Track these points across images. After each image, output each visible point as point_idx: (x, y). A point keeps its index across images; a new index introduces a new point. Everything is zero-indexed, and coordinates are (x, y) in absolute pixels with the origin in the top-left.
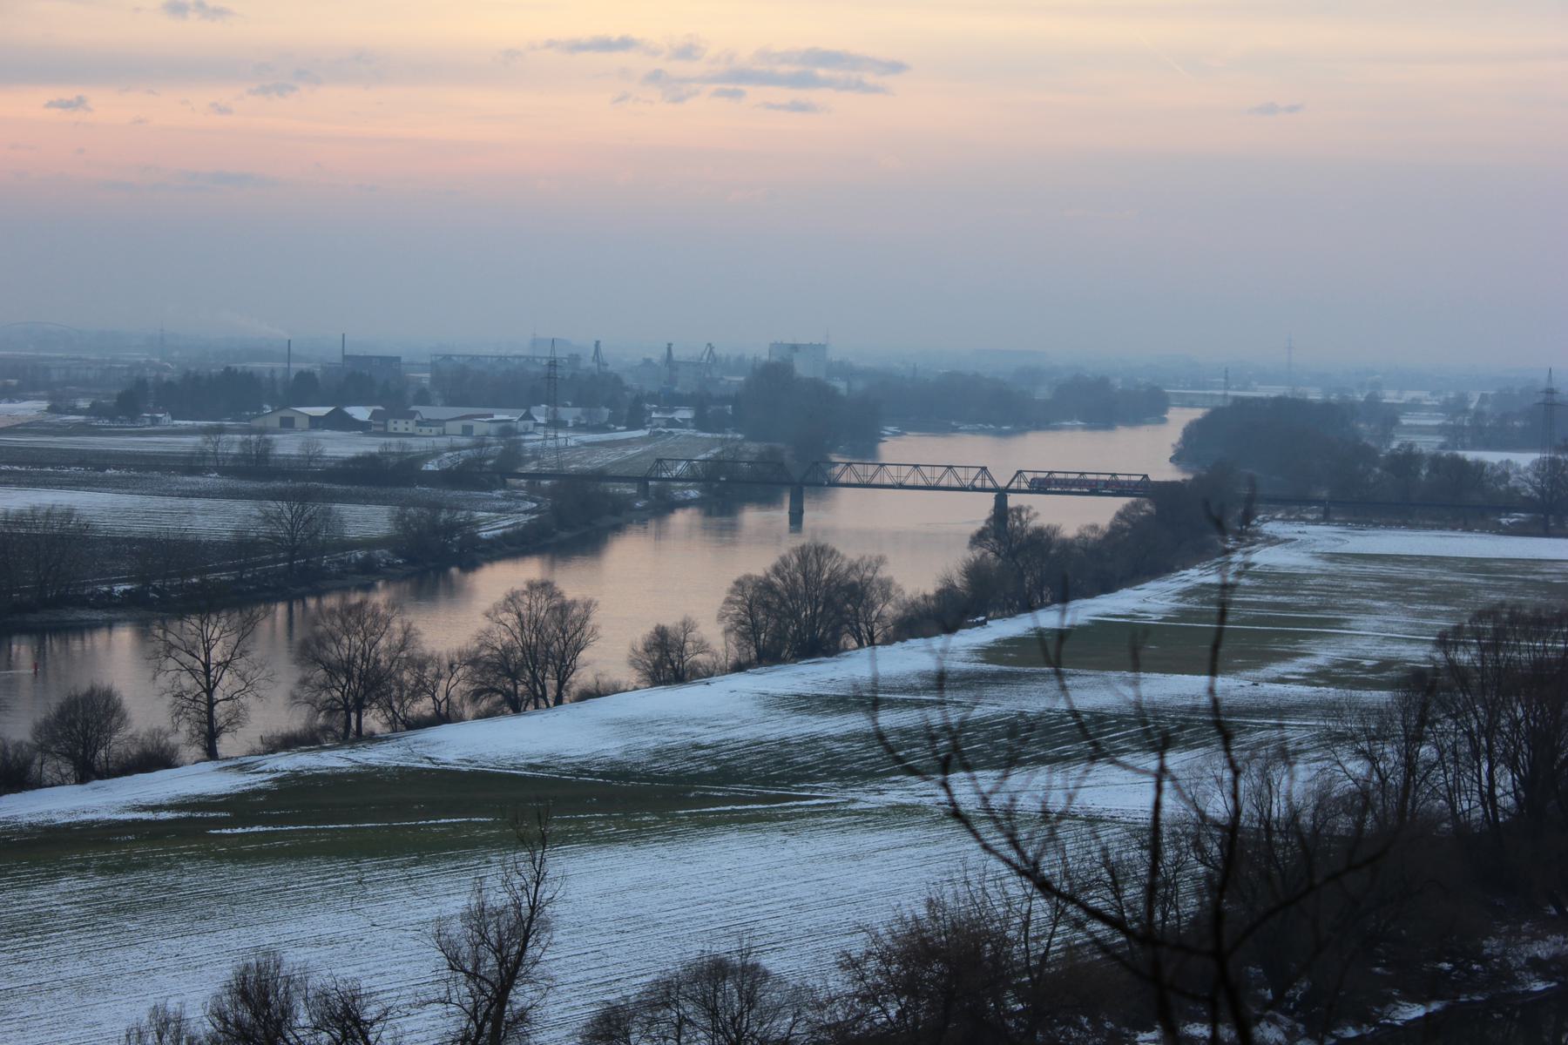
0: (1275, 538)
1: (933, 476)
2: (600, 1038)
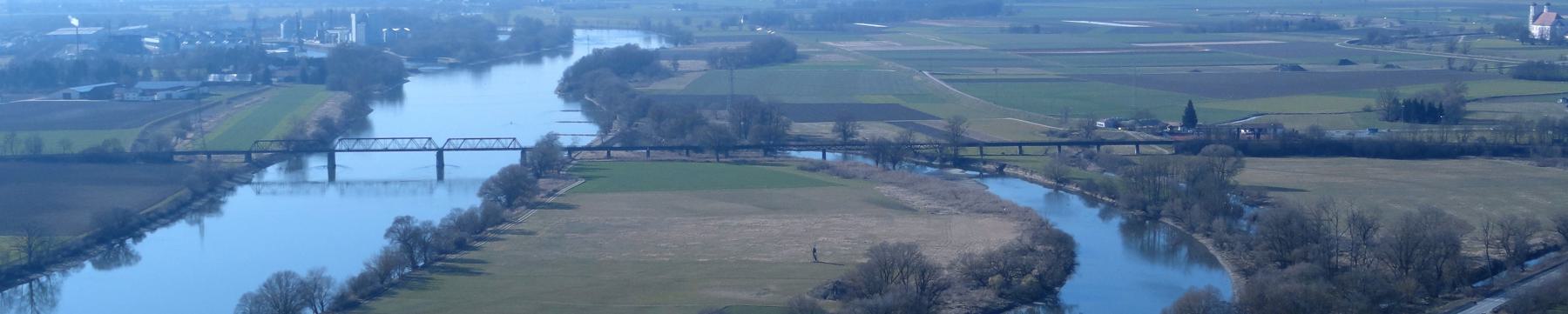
1: (493, 144)
2: (337, 310)
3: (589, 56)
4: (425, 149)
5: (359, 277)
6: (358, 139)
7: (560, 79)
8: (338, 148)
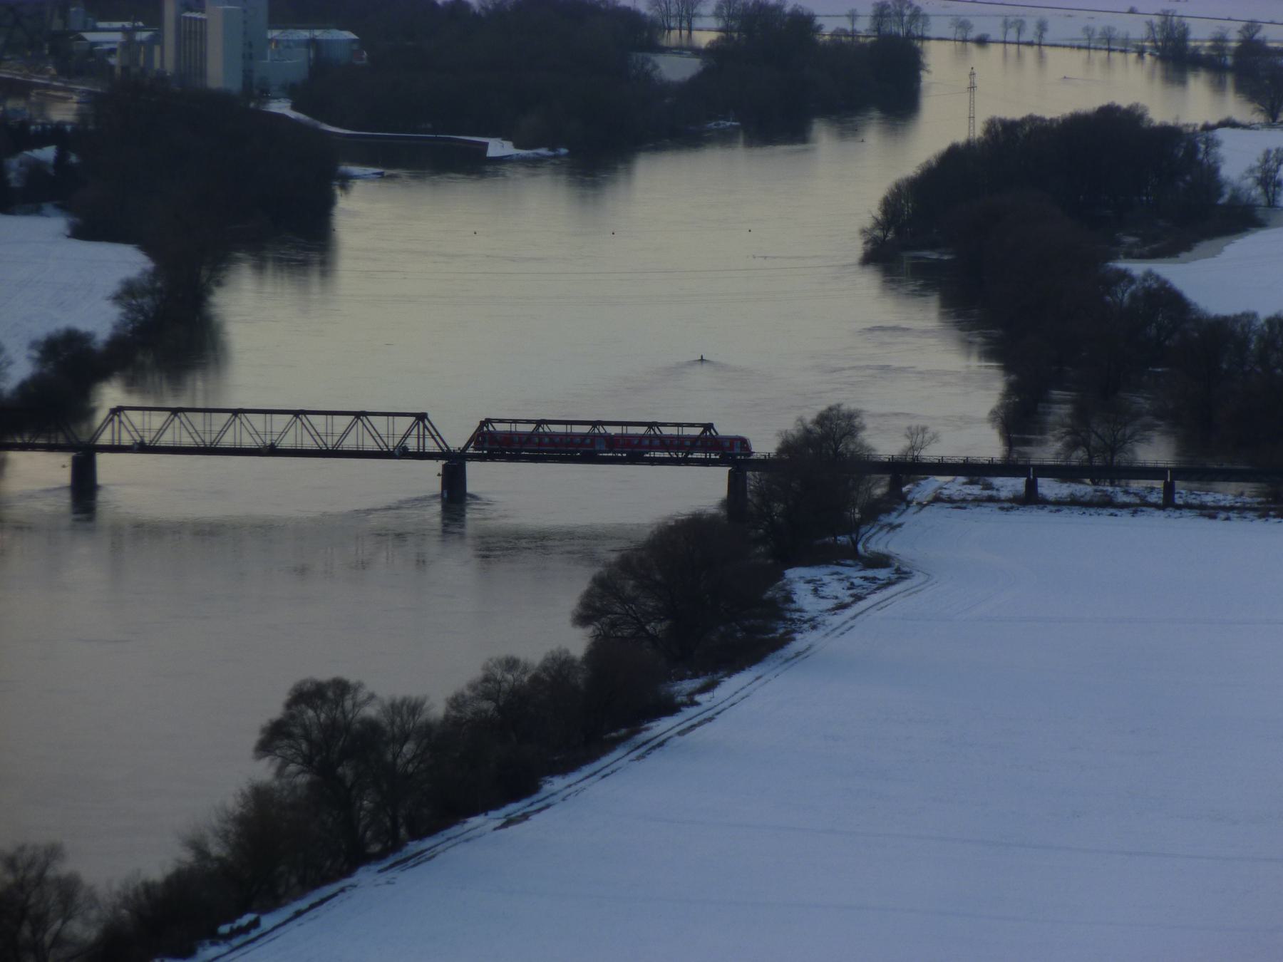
0: (799, 652)
3: (969, 145)
4: (403, 453)
5: (544, 668)
6: (175, 411)
7: (868, 223)
8: (105, 439)
